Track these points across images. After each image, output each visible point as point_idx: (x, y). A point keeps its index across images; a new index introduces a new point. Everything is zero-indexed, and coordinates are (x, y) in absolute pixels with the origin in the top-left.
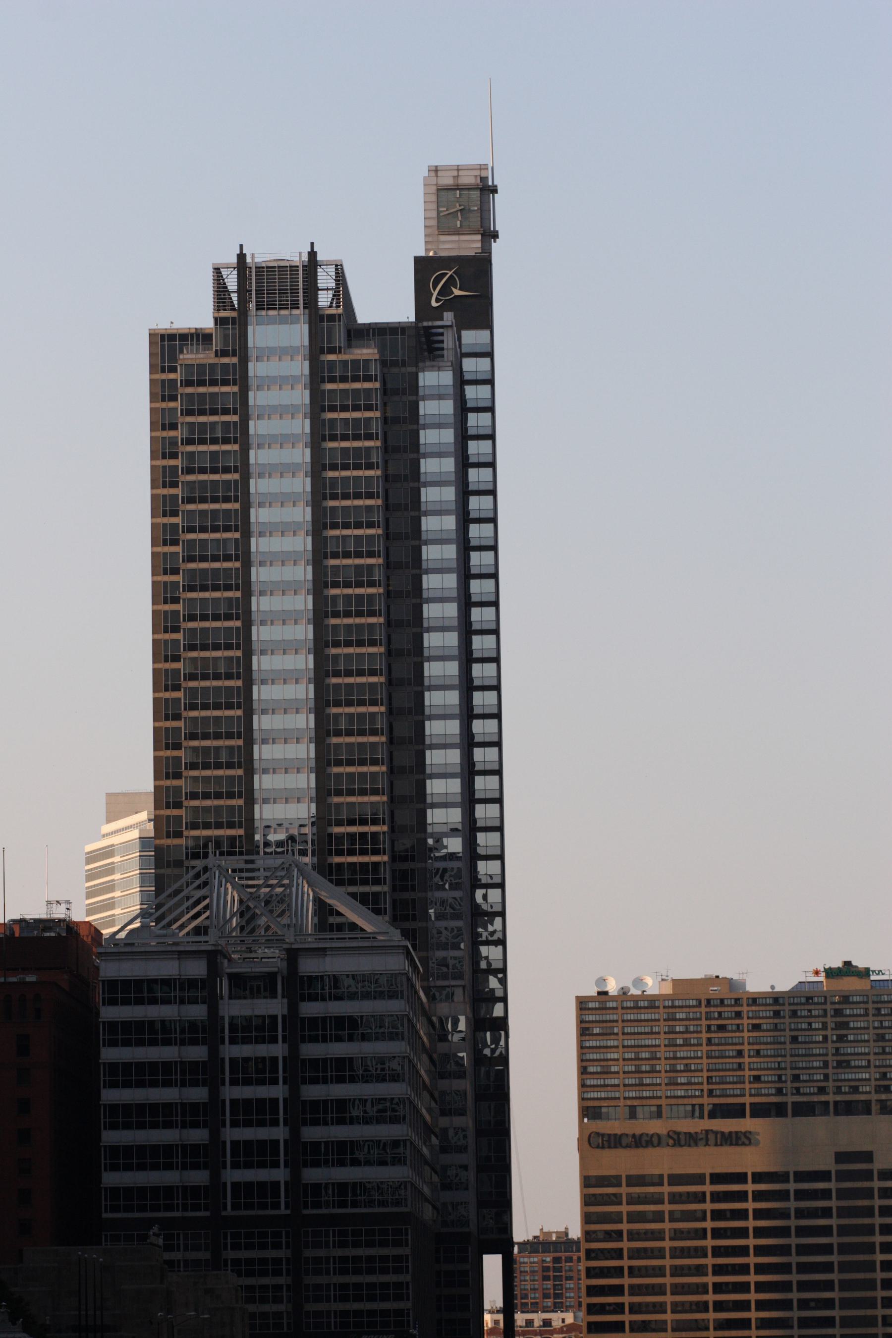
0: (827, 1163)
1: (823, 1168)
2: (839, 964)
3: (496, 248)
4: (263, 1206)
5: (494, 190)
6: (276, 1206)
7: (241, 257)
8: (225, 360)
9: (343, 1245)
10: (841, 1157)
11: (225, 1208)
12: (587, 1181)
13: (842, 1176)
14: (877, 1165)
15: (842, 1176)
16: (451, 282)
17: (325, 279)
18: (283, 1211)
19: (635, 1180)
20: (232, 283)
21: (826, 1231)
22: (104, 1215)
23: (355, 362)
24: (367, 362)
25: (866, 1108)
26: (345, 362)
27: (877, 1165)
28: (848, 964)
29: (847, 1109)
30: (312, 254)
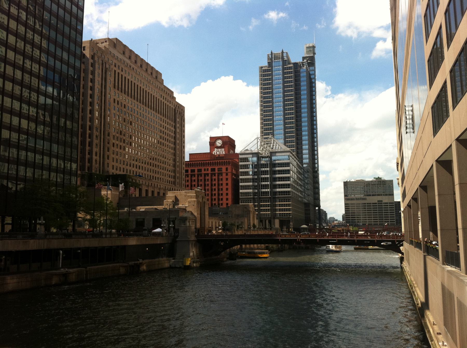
0: (377, 202)
1: (376, 202)
2: (377, 177)
3: (316, 56)
4: (266, 195)
5: (315, 47)
6: (268, 195)
7: (272, 52)
8: (269, 68)
9: (280, 202)
10: (378, 201)
11: (260, 196)
12: (345, 204)
13: (378, 203)
14: (383, 202)
15: (378, 203)
16: (308, 60)
17: (285, 55)
18: (270, 196)
19: (351, 204)
20: (270, 56)
21: (377, 210)
22: (240, 197)
23: (289, 67)
24: (291, 67)
25: (381, 195)
26: (288, 67)
27: (383, 202)
28: (378, 177)
29: (378, 195)
30: (282, 51)
